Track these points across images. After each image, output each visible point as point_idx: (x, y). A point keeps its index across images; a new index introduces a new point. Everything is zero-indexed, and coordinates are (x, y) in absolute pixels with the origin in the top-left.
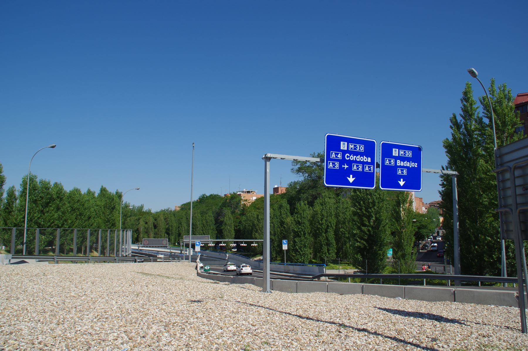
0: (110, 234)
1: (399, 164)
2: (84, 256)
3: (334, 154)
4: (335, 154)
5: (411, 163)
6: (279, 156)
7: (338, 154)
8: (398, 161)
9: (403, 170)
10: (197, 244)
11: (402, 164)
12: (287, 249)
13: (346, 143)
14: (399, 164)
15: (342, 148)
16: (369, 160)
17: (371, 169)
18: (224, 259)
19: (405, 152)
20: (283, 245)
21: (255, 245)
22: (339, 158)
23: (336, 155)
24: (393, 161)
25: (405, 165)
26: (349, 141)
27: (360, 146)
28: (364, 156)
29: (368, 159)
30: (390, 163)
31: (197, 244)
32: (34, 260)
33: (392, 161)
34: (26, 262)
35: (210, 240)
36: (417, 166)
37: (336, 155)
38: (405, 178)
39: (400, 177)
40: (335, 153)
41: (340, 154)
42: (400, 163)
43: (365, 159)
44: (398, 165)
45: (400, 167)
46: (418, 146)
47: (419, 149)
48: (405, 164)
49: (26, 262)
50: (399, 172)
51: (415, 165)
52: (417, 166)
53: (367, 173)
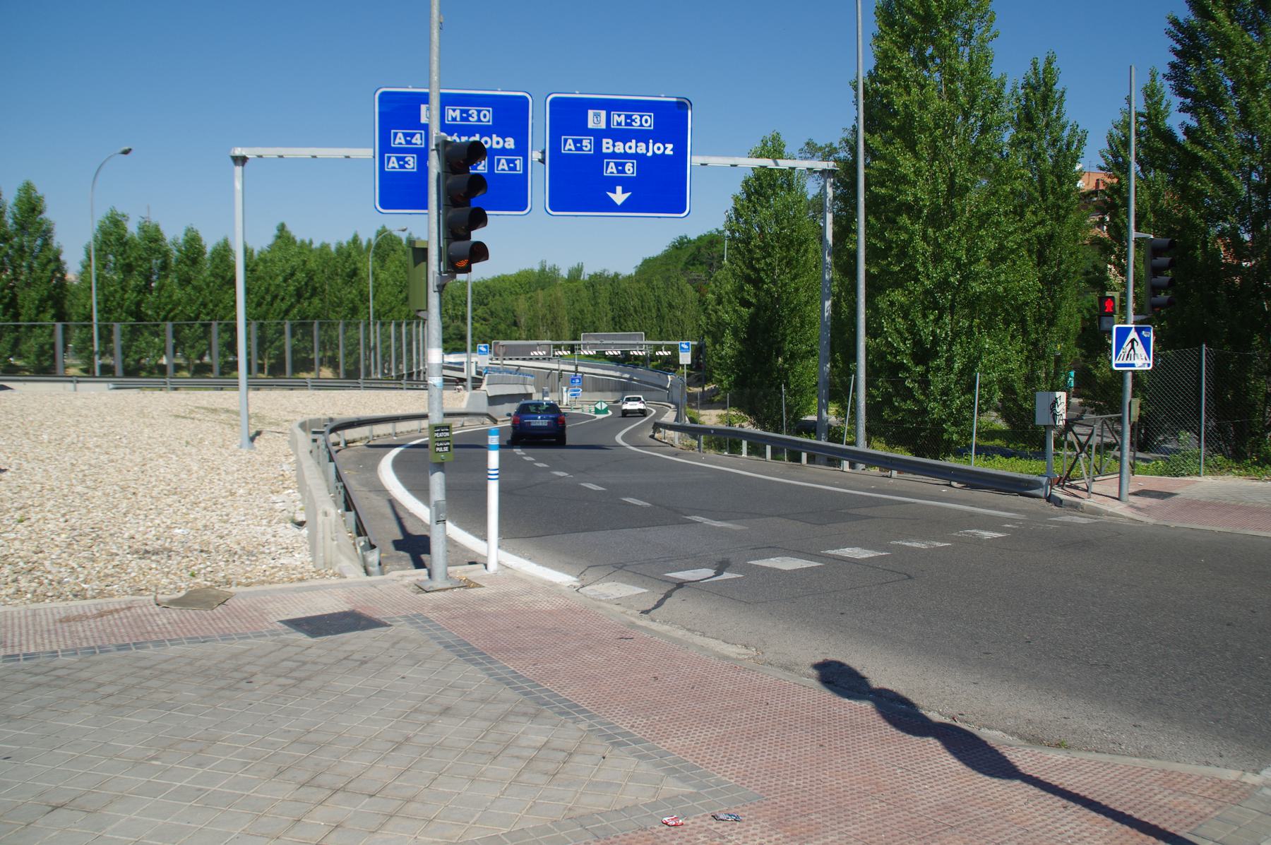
0: (345, 332)
1: (608, 148)
2: (85, 375)
3: (570, 141)
4: (405, 135)
5: (651, 145)
6: (271, 152)
7: (413, 135)
8: (605, 141)
9: (623, 165)
10: (682, 348)
11: (620, 147)
12: (690, 363)
13: (603, 113)
14: (608, 148)
15: (591, 125)
16: (510, 143)
17: (515, 165)
18: (660, 387)
19: (627, 117)
20: (680, 354)
21: (565, 353)
22: (416, 144)
23: (409, 138)
24: (587, 144)
25: (629, 151)
26: (610, 106)
27: (479, 112)
28: (494, 136)
29: (504, 142)
30: (580, 149)
31: (683, 348)
32: (104, 385)
33: (585, 143)
34: (8, 388)
35: (644, 342)
36: (671, 153)
37: (409, 138)
38: (627, 184)
39: (612, 183)
40: (574, 140)
41: (418, 136)
42: (614, 146)
43: (498, 143)
44: (604, 150)
45: (614, 155)
46: (675, 100)
47: (681, 108)
48: (630, 148)
49: (8, 388)
50: (611, 170)
51: (665, 148)
52: (671, 153)
53: (503, 177)
